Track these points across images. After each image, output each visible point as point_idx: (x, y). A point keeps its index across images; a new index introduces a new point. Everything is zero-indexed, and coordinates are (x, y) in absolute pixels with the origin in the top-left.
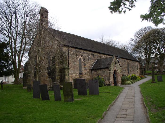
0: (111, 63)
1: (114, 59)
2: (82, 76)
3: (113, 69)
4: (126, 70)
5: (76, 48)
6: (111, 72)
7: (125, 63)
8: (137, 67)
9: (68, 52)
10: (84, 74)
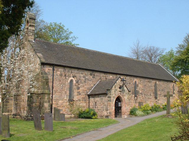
0: (112, 87)
1: (117, 82)
2: (73, 104)
3: (115, 95)
4: (150, 95)
5: (66, 66)
6: (110, 100)
7: (150, 85)
8: (172, 90)
9: (53, 72)
10: (77, 101)
